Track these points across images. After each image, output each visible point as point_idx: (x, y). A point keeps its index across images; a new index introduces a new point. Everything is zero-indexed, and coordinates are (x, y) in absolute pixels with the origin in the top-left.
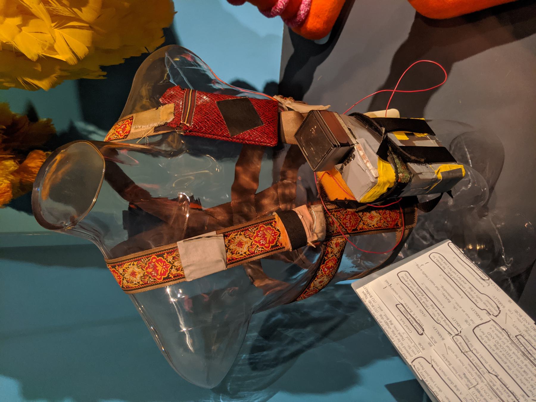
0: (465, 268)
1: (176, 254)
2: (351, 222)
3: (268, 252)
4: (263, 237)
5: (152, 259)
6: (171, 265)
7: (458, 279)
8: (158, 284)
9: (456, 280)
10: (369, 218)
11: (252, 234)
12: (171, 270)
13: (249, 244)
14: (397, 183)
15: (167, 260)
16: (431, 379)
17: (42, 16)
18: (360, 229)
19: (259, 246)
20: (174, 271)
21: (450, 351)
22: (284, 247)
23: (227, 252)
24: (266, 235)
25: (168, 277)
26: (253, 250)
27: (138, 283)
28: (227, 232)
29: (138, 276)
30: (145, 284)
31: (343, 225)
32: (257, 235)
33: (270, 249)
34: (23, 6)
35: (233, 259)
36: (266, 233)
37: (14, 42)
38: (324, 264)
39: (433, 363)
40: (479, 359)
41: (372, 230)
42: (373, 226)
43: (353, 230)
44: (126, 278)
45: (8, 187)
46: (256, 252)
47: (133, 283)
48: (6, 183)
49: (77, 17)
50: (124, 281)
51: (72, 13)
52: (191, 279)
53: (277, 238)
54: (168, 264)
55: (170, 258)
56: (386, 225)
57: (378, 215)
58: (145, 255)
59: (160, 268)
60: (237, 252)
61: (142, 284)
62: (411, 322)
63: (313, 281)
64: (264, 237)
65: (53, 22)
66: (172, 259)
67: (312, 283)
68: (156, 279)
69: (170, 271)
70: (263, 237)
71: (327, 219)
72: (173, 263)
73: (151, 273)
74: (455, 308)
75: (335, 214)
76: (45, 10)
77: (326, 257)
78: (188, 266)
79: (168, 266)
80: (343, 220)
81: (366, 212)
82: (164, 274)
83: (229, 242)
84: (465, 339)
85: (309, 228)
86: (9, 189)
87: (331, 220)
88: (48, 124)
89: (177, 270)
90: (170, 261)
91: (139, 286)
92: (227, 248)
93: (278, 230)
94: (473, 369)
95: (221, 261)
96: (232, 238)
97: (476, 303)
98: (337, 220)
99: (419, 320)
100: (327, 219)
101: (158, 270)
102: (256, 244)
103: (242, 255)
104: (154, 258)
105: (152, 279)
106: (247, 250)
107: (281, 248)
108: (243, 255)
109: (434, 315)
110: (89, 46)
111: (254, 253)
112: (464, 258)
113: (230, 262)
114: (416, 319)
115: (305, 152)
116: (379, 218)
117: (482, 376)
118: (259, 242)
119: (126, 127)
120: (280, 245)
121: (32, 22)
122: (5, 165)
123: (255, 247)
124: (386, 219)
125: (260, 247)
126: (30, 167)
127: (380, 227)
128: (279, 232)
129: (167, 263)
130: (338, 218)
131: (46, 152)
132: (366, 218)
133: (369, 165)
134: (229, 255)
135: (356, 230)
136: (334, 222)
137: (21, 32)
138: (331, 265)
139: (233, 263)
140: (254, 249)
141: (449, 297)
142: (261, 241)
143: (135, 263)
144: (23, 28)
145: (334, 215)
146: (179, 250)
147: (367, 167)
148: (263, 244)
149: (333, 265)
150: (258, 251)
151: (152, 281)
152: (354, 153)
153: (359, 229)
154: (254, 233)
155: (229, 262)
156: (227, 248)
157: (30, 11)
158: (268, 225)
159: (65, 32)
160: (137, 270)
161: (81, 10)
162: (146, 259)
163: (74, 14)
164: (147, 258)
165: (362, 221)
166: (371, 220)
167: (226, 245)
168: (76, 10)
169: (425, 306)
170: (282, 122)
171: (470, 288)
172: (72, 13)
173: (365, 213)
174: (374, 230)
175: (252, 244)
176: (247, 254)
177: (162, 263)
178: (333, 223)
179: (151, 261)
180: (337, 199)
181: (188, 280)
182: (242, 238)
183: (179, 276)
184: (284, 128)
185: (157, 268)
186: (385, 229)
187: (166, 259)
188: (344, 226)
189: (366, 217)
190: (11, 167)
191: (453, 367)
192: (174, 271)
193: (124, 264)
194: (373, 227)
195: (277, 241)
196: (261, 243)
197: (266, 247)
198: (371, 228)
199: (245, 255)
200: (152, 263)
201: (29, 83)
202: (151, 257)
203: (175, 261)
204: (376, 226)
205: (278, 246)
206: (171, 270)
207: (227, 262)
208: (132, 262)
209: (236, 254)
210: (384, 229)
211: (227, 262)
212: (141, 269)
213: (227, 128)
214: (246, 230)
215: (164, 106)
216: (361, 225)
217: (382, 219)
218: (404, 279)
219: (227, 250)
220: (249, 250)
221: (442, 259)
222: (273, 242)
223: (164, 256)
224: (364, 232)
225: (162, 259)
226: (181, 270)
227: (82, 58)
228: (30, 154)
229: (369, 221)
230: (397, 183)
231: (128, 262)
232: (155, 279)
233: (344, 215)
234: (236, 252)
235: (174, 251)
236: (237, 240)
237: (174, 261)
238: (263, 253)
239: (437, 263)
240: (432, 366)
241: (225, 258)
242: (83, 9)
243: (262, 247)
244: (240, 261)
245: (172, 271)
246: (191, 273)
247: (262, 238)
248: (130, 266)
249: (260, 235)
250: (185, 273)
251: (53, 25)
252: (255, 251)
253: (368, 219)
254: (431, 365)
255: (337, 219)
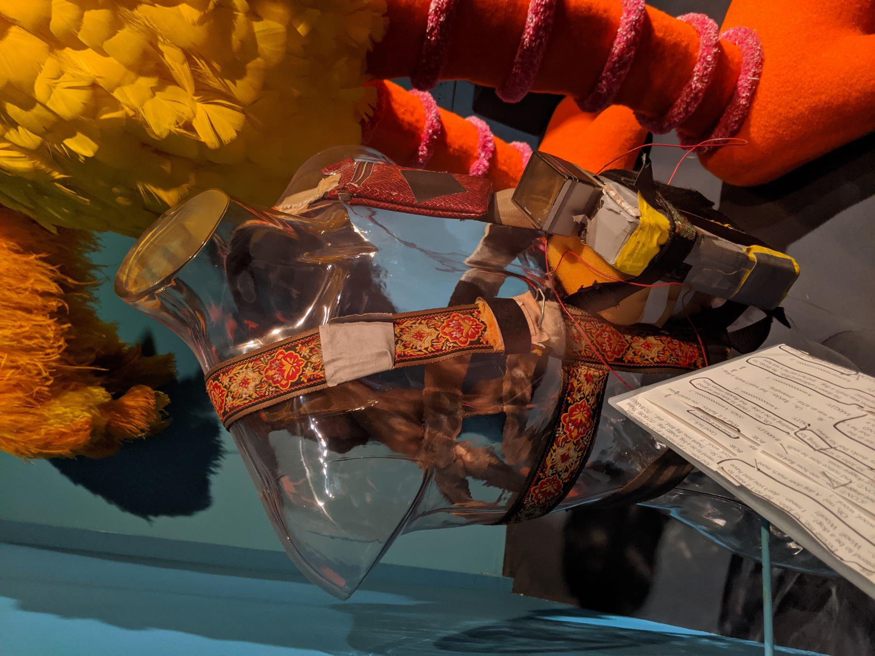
0: (813, 367)
1: (315, 344)
2: (612, 344)
3: (463, 350)
4: (457, 329)
5: (277, 356)
6: (306, 361)
7: (802, 378)
8: (282, 395)
9: (797, 379)
10: (644, 346)
11: (439, 324)
12: (304, 369)
13: (434, 337)
14: (673, 233)
15: (301, 355)
16: (757, 483)
17: (188, 89)
18: (629, 362)
19: (450, 339)
20: (309, 371)
21: (793, 450)
22: (492, 347)
23: (396, 343)
24: (462, 326)
25: (299, 382)
26: (440, 345)
27: (250, 396)
28: (400, 319)
29: (252, 385)
30: (261, 397)
31: (597, 345)
32: (448, 325)
33: (469, 345)
34: (164, 63)
35: (405, 355)
36: (462, 323)
37: (143, 110)
38: (567, 412)
39: (760, 467)
40: (853, 456)
41: (650, 367)
42: (653, 359)
43: (616, 360)
44: (231, 392)
45: (87, 423)
46: (444, 348)
47: (241, 398)
48: (87, 417)
49: (229, 93)
50: (227, 399)
51: (223, 85)
52: (336, 383)
53: (480, 332)
54: (301, 360)
55: (305, 351)
56: (675, 360)
57: (659, 342)
58: (268, 351)
59: (288, 368)
60: (413, 345)
61: (256, 398)
62: (717, 427)
63: (550, 451)
64: (459, 328)
65: (195, 95)
66: (308, 351)
67: (547, 456)
68: (279, 386)
69: (303, 371)
70: (457, 329)
71: (568, 328)
72: (310, 358)
73: (272, 378)
74: (797, 407)
75: (581, 322)
76: (188, 72)
77: (569, 398)
78: (333, 361)
79: (300, 363)
80: (597, 337)
81: (637, 336)
82: (293, 377)
83: (401, 331)
84: (819, 434)
85: (534, 320)
86: (87, 426)
87: (574, 331)
88: (169, 360)
89: (315, 368)
90: (306, 354)
91: (250, 401)
92: (396, 339)
93: (483, 322)
94: (839, 467)
95: (386, 353)
96: (407, 327)
97: (837, 399)
98: (586, 334)
99: (729, 421)
100: (568, 328)
101: (285, 370)
102: (445, 337)
103: (420, 351)
104: (281, 353)
105: (273, 387)
106: (430, 345)
107: (486, 348)
108: (422, 351)
109: (759, 417)
110: (238, 130)
111: (441, 350)
112: (811, 359)
113: (401, 358)
114: (725, 421)
115: (528, 211)
116: (661, 348)
117: (857, 473)
118: (450, 334)
119: (282, 365)
120: (484, 343)
121: (171, 88)
122: (91, 393)
123: (444, 340)
124: (673, 350)
125: (451, 341)
126: (128, 406)
127: (665, 362)
128: (485, 325)
129: (300, 358)
130: (588, 331)
131: (156, 391)
132: (638, 346)
133: (624, 205)
134: (400, 349)
135: (621, 360)
136: (580, 336)
137: (154, 98)
138: (579, 418)
139: (405, 361)
140: (441, 343)
141: (784, 397)
142: (454, 333)
143: (250, 365)
144: (157, 93)
145: (580, 324)
146: (322, 339)
147: (623, 208)
148: (456, 337)
149: (584, 420)
150: (447, 348)
151: (272, 392)
152: (602, 199)
153: (626, 361)
154: (443, 322)
155: (398, 359)
156: (396, 339)
157: (171, 73)
158: (467, 314)
159: (210, 108)
160: (251, 375)
161: (235, 83)
162: (267, 357)
163: (224, 87)
164: (270, 355)
165: (630, 348)
166: (648, 349)
167: (395, 335)
168: (228, 82)
169: (741, 409)
170: (497, 203)
171: (824, 384)
172: (223, 85)
173: (636, 338)
174: (654, 367)
175: (439, 336)
176: (429, 350)
177: (293, 359)
178: (580, 337)
179: (275, 358)
180: (582, 288)
181: (330, 385)
182: (424, 328)
183: (317, 379)
184: (499, 209)
185: (283, 369)
186: (674, 367)
187: (298, 352)
188: (599, 347)
189: (639, 343)
190: (98, 395)
191: (798, 465)
192: (309, 370)
193: (233, 368)
194: (651, 361)
195: (481, 336)
196: (454, 336)
197: (461, 342)
198: (647, 362)
199: (427, 352)
200: (277, 362)
201: (151, 194)
202: (276, 352)
203: (313, 355)
204: (656, 359)
205: (482, 343)
206: (304, 369)
207: (395, 359)
208: (245, 364)
209: (412, 348)
210: (671, 367)
211: (395, 359)
212: (257, 373)
213: (412, 193)
214: (430, 318)
215: (327, 179)
216: (630, 355)
217: (667, 350)
218: (703, 386)
219: (398, 340)
220: (432, 346)
221: (770, 362)
222: (473, 336)
223: (297, 348)
224: (637, 367)
225: (294, 352)
226: (321, 370)
227: (227, 143)
228: (131, 389)
229: (644, 351)
230: (673, 233)
231: (240, 365)
232: (276, 387)
233: (598, 330)
234: (411, 346)
235: (313, 340)
236: (414, 331)
237: (311, 354)
238: (456, 351)
239: (762, 366)
240: (759, 470)
241: (393, 350)
242: (238, 82)
243: (454, 341)
244: (417, 359)
245: (307, 371)
246: (336, 372)
247: (455, 330)
248: (241, 371)
249: (452, 325)
250: (327, 374)
251: (196, 98)
252: (442, 347)
253: (642, 348)
254: (756, 469)
255: (586, 332)
